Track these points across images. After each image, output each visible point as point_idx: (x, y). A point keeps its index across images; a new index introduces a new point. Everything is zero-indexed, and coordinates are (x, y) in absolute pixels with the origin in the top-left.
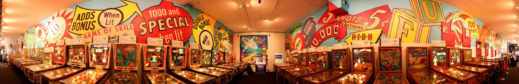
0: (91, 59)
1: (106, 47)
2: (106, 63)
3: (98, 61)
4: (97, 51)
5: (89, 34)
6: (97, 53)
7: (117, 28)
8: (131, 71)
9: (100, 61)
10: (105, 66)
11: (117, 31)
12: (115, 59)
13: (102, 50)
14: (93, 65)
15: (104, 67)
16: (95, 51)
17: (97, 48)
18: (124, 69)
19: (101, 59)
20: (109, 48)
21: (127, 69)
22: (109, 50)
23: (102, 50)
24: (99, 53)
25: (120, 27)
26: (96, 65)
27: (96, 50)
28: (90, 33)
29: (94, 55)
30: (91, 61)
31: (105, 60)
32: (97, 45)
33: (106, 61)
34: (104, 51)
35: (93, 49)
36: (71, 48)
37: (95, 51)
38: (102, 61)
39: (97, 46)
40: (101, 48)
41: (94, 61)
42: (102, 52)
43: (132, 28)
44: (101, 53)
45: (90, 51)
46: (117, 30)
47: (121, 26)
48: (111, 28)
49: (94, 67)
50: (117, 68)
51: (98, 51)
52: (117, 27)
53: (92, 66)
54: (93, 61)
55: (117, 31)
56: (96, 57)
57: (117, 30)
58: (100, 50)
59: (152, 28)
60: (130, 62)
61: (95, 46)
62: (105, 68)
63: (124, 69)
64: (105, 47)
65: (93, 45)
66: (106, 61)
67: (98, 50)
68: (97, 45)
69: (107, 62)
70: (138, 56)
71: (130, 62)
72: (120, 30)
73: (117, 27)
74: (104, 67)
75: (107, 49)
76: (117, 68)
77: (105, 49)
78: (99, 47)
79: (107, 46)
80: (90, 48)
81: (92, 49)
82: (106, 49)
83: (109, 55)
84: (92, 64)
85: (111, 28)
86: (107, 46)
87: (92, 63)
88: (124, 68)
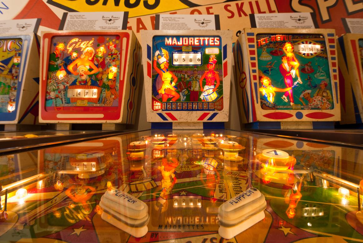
0: (155, 91)
1: (214, 46)
2: (218, 104)
3: (183, 98)
4: (179, 59)
5: (139, 21)
6: (180, 66)
7: (229, 8)
8: (314, 122)
9: (194, 96)
10: (215, 115)
11: (229, 17)
12: (336, 83)
13: (199, 56)
14: (164, 113)
15: (211, 118)
16: (171, 60)
17: (179, 49)
18: (294, 119)
19: (197, 89)
20: (225, 47)
21: (305, 119)
22: (225, 57)
23: (199, 56)
24: (187, 66)
25: (237, 5)
26: (174, 113)
27: (176, 56)
28: (142, 18)
29: (167, 76)
30: (153, 100)
31: (211, 91)
32: (178, 40)
33: (214, 96)
34: (205, 59)
35: (164, 51)
36: (254, 148)
37: (171, 60)
38: (202, 97)
39: (180, 43)
40: (195, 49)
41: (169, 99)
42: (199, 63)
43: (273, 9)
44: (196, 66)
45: (149, 57)
46: (230, 15)
47: (242, 4)
48: (211, 8)
49: (170, 120)
50: (266, 116)
51: (184, 60)
52: (230, 5)
53: (159, 120)
54: (161, 100)
55: (229, 17)
56: (174, 84)
57: (230, 15)
58: (191, 55)
59: (328, 8)
60: (309, 91)
61: (169, 41)
62: (215, 120)
63: (294, 119)
64: (209, 46)
65: (163, 37)
66: (214, 96)
67: (184, 55)
68: (178, 40)
69: (220, 99)
70: (254, 71)
71: (309, 91)
72: (240, 16)
73: (230, 5)
74: (211, 118)
75: (216, 51)
76: (266, 116)
77: (208, 51)
78: (188, 45)
79: (217, 43)
80: (149, 47)
81: (157, 53)
82: (213, 52)
83: (226, 74)
84: (160, 112)
85: (211, 8)
86: (217, 43)
87: (158, 105)
88: (293, 112)
